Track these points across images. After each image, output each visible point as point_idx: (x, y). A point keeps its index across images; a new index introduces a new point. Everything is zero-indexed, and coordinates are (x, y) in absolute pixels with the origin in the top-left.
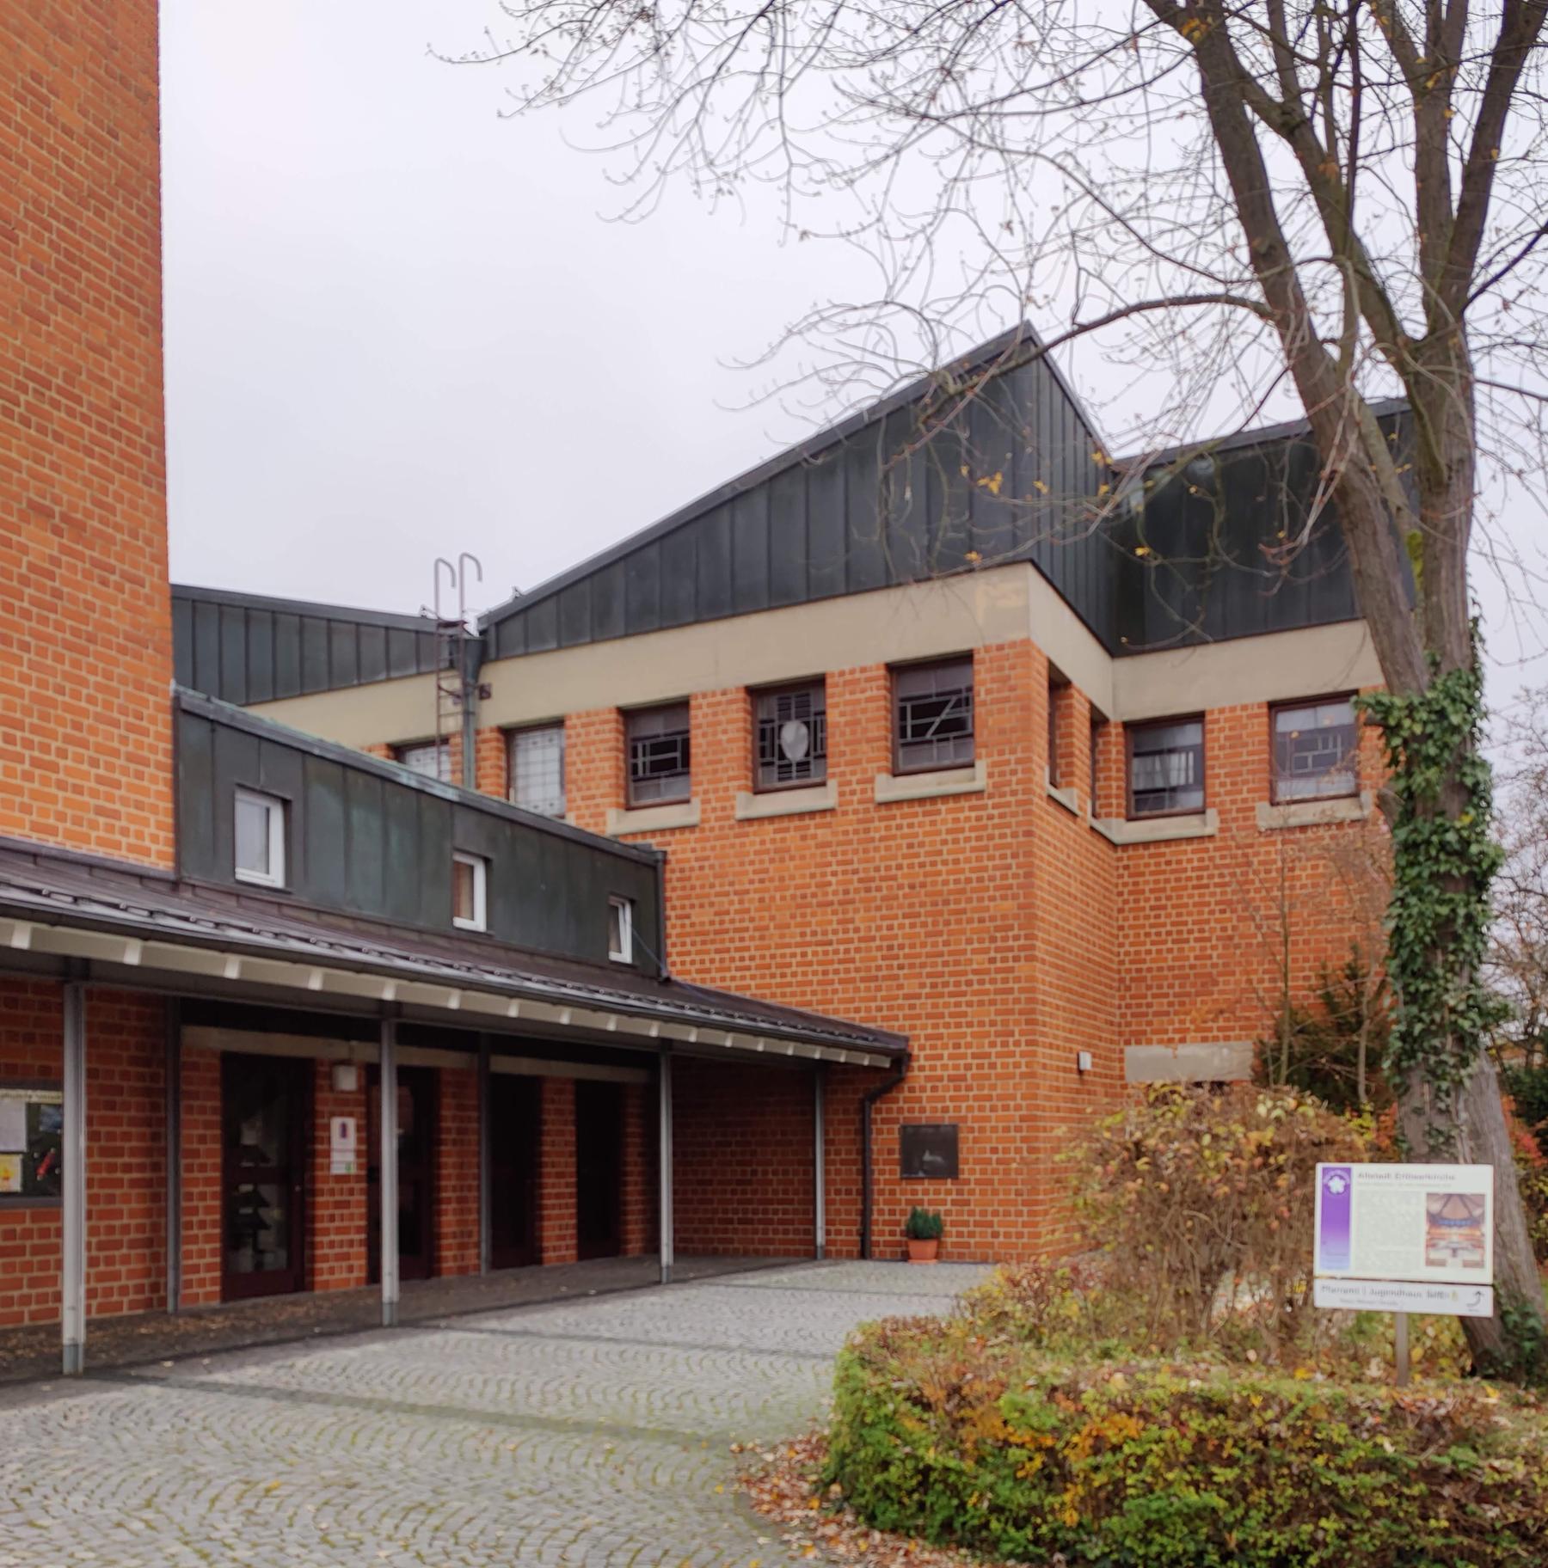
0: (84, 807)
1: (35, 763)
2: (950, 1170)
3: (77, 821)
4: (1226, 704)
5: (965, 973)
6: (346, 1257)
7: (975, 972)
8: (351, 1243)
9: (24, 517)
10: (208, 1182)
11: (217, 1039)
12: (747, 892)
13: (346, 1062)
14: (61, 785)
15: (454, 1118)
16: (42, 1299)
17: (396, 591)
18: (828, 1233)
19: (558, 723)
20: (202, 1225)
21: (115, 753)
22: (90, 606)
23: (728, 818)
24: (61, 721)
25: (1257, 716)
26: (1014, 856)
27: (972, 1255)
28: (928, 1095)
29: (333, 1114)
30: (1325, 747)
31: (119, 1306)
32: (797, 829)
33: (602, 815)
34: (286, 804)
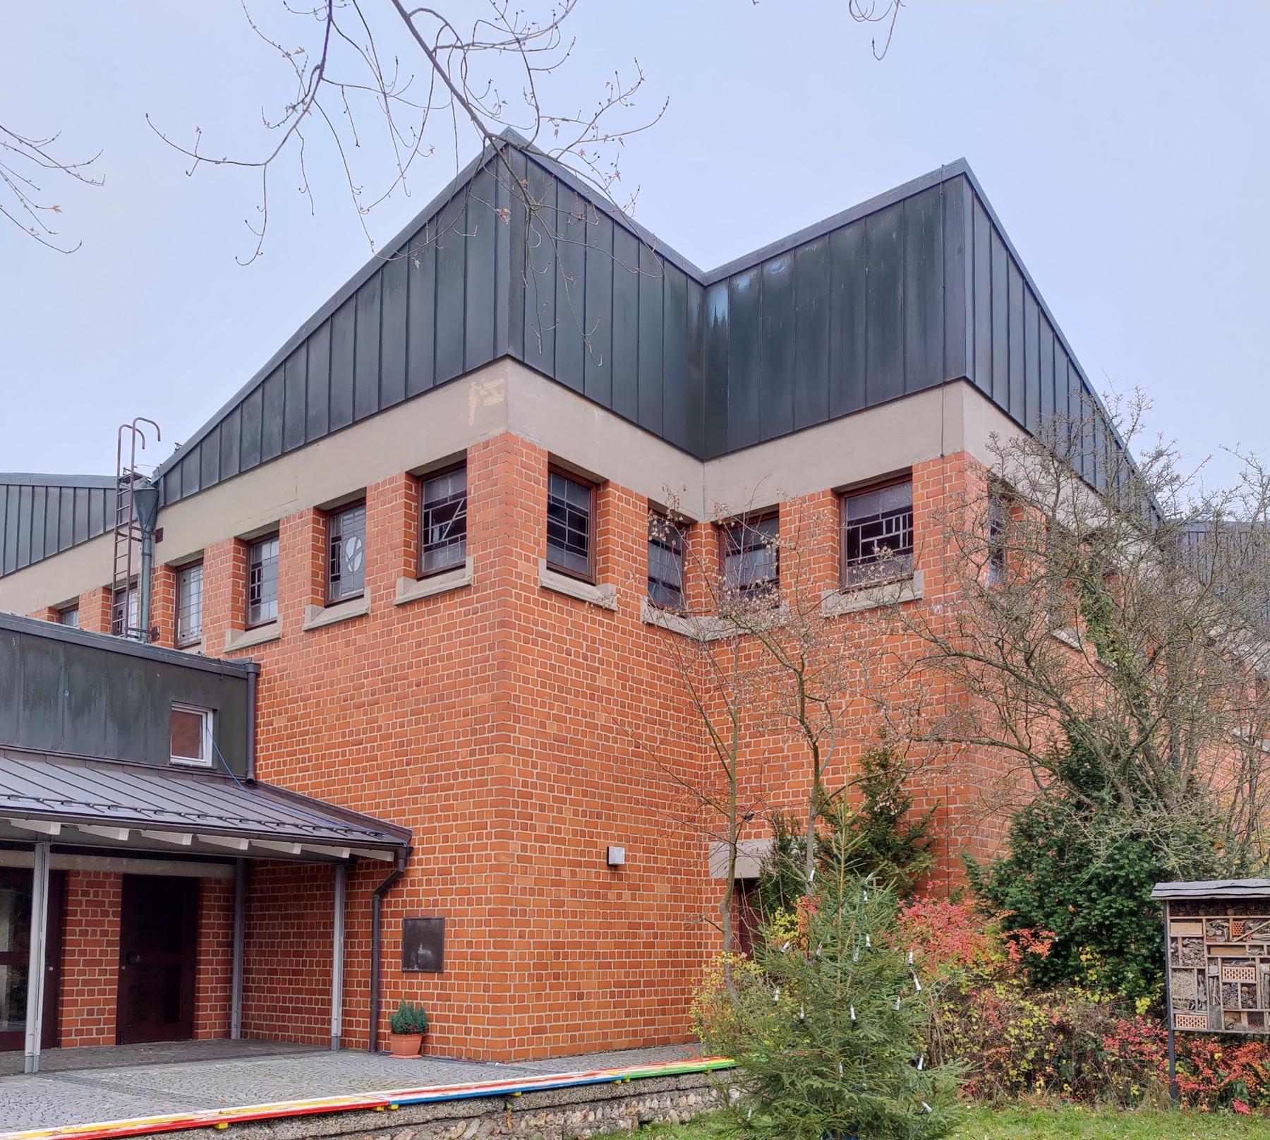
2: (435, 966)
5: (452, 766)
7: (460, 765)
18: (344, 1023)
25: (822, 504)
26: (492, 648)
27: (451, 1051)
28: (423, 892)
30: (889, 530)
32: (343, 636)
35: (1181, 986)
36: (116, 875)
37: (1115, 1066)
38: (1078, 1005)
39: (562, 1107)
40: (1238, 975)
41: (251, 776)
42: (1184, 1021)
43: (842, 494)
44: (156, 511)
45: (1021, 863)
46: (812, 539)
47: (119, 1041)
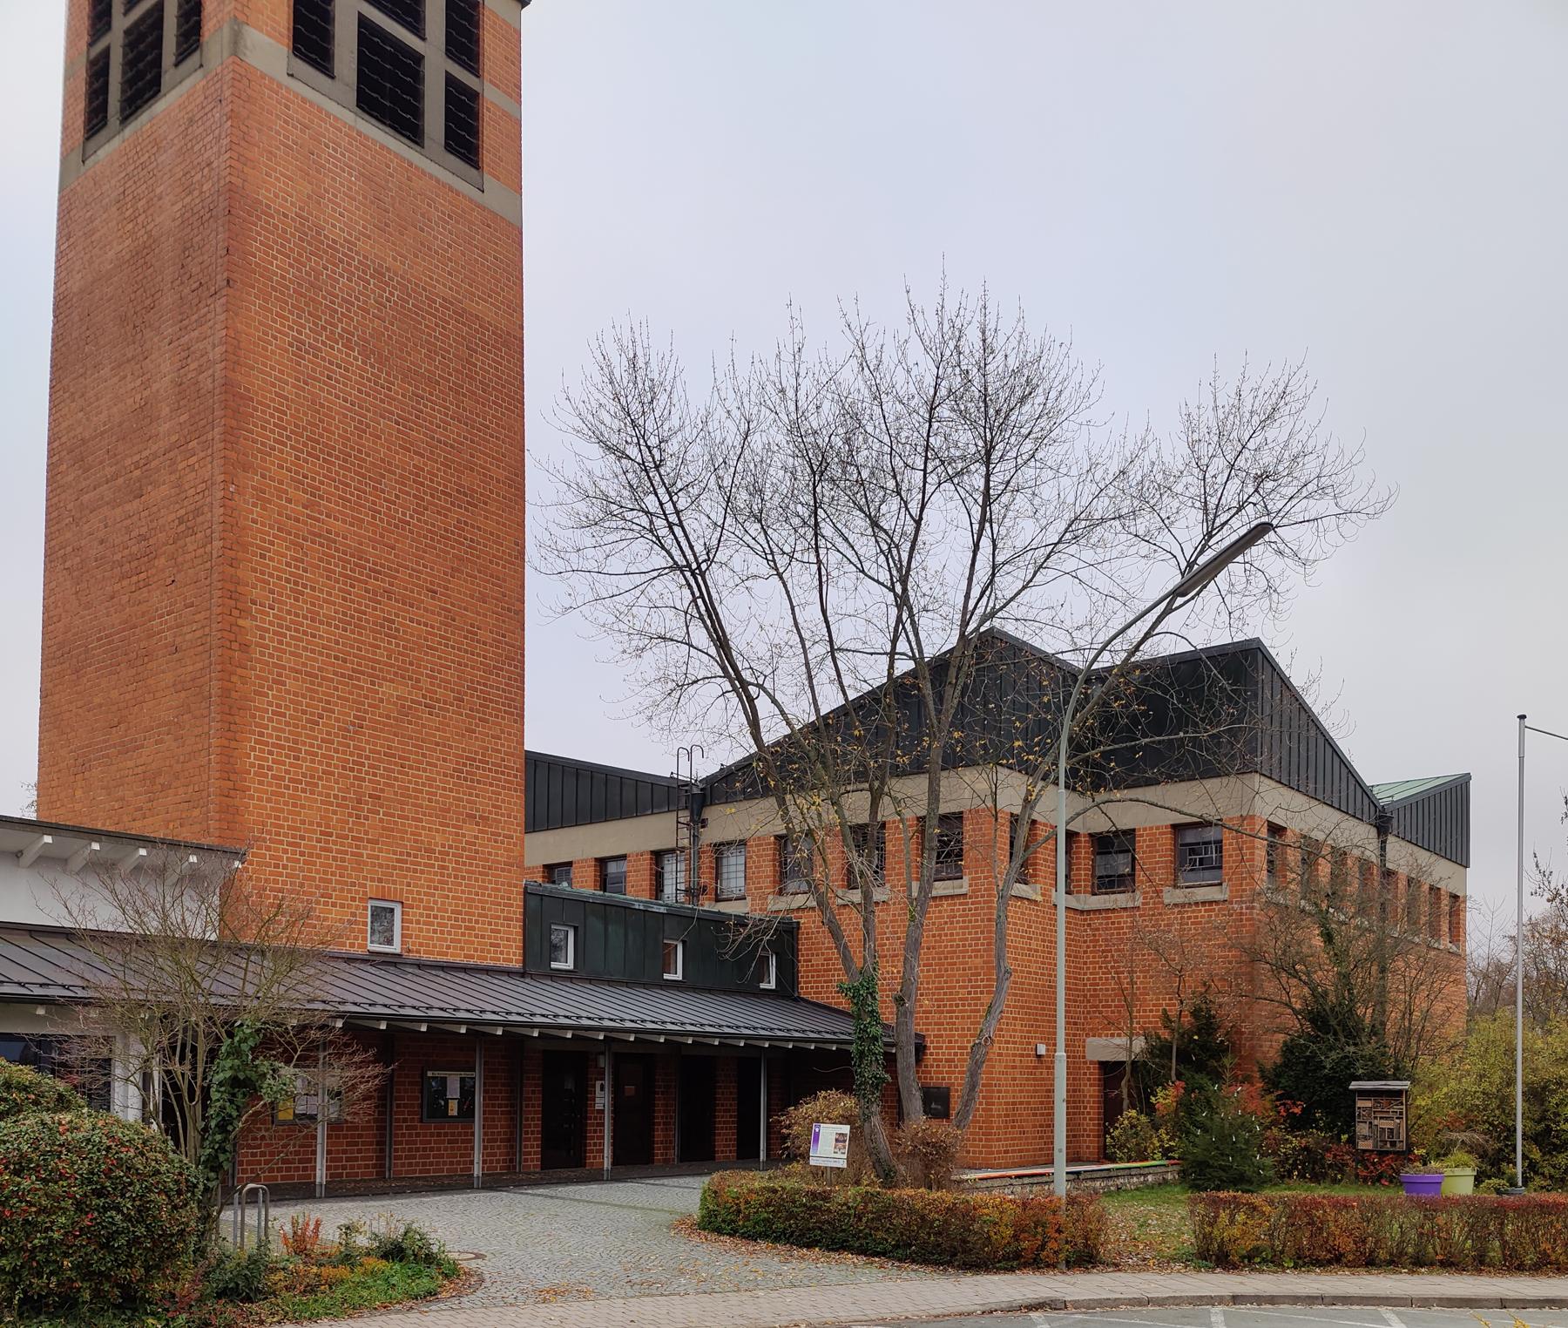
4: (1147, 825)
10: (536, 1112)
14: (476, 936)
16: (465, 1163)
19: (743, 843)
34: (576, 929)
35: (1362, 1129)
37: (1330, 1166)
38: (1313, 1138)
39: (1093, 1179)
40: (1386, 1124)
42: (1362, 1145)
43: (1177, 828)
45: (1286, 1065)
46: (1155, 855)
47: (681, 1160)
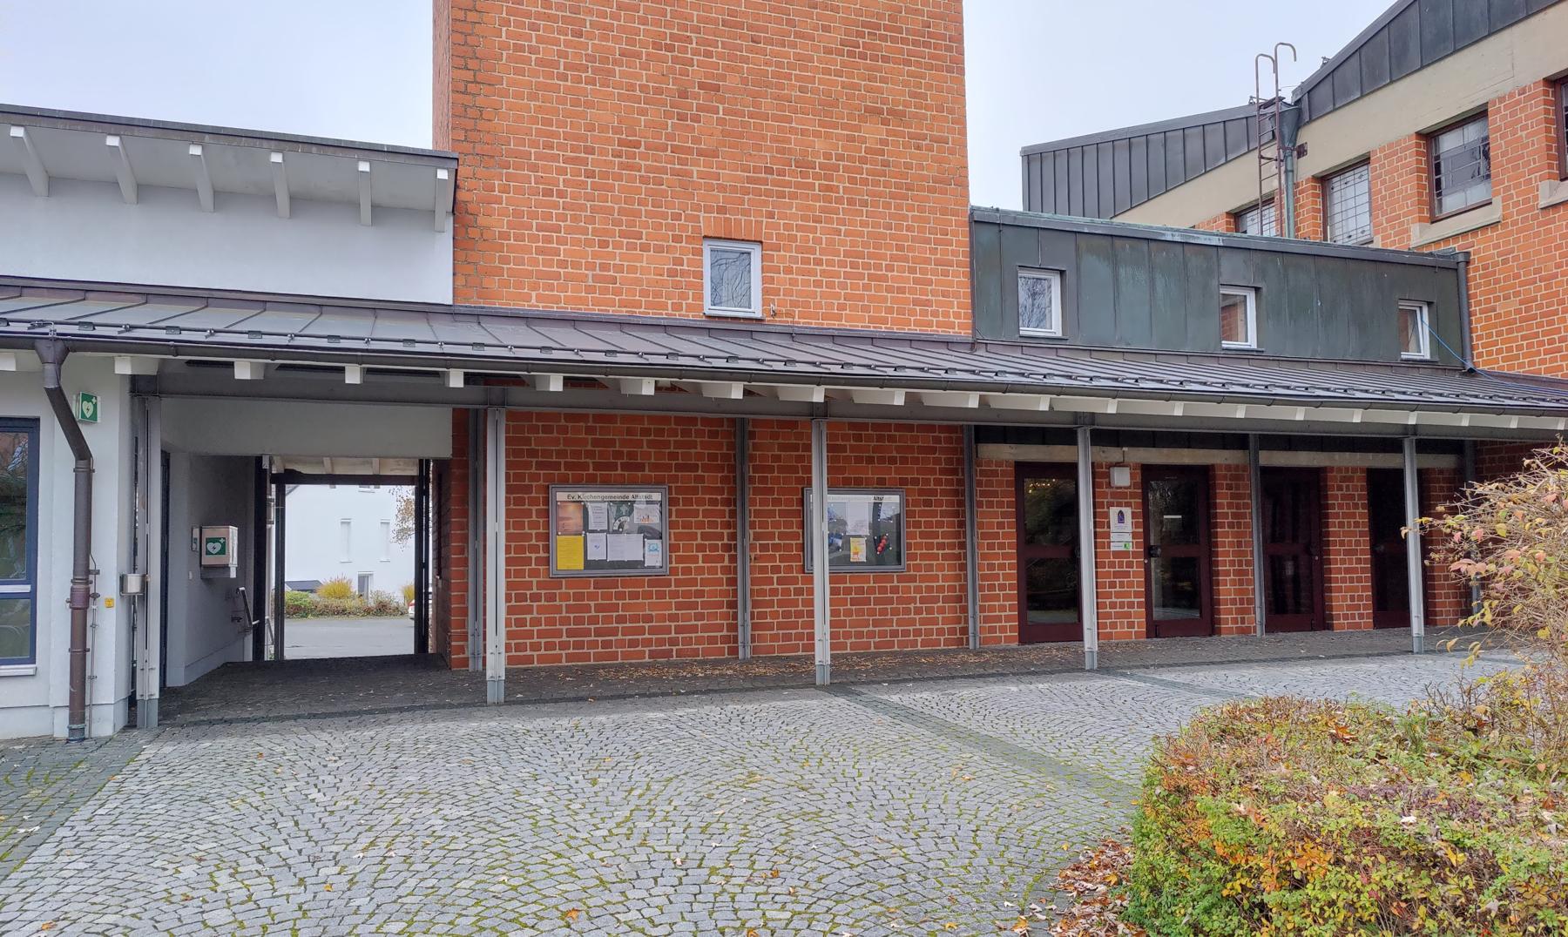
0: (906, 301)
1: (871, 277)
3: (901, 311)
6: (1128, 615)
8: (1131, 605)
9: (862, 119)
11: (1008, 453)
12: (1555, 276)
13: (1118, 465)
15: (1230, 506)
17: (1227, 89)
19: (1364, 161)
20: (1002, 587)
21: (927, 261)
22: (908, 166)
23: (1532, 208)
24: (888, 247)
29: (1111, 505)
31: (891, 644)
33: (1407, 231)
36: (1362, 470)
41: (1469, 365)
44: (1299, 124)
